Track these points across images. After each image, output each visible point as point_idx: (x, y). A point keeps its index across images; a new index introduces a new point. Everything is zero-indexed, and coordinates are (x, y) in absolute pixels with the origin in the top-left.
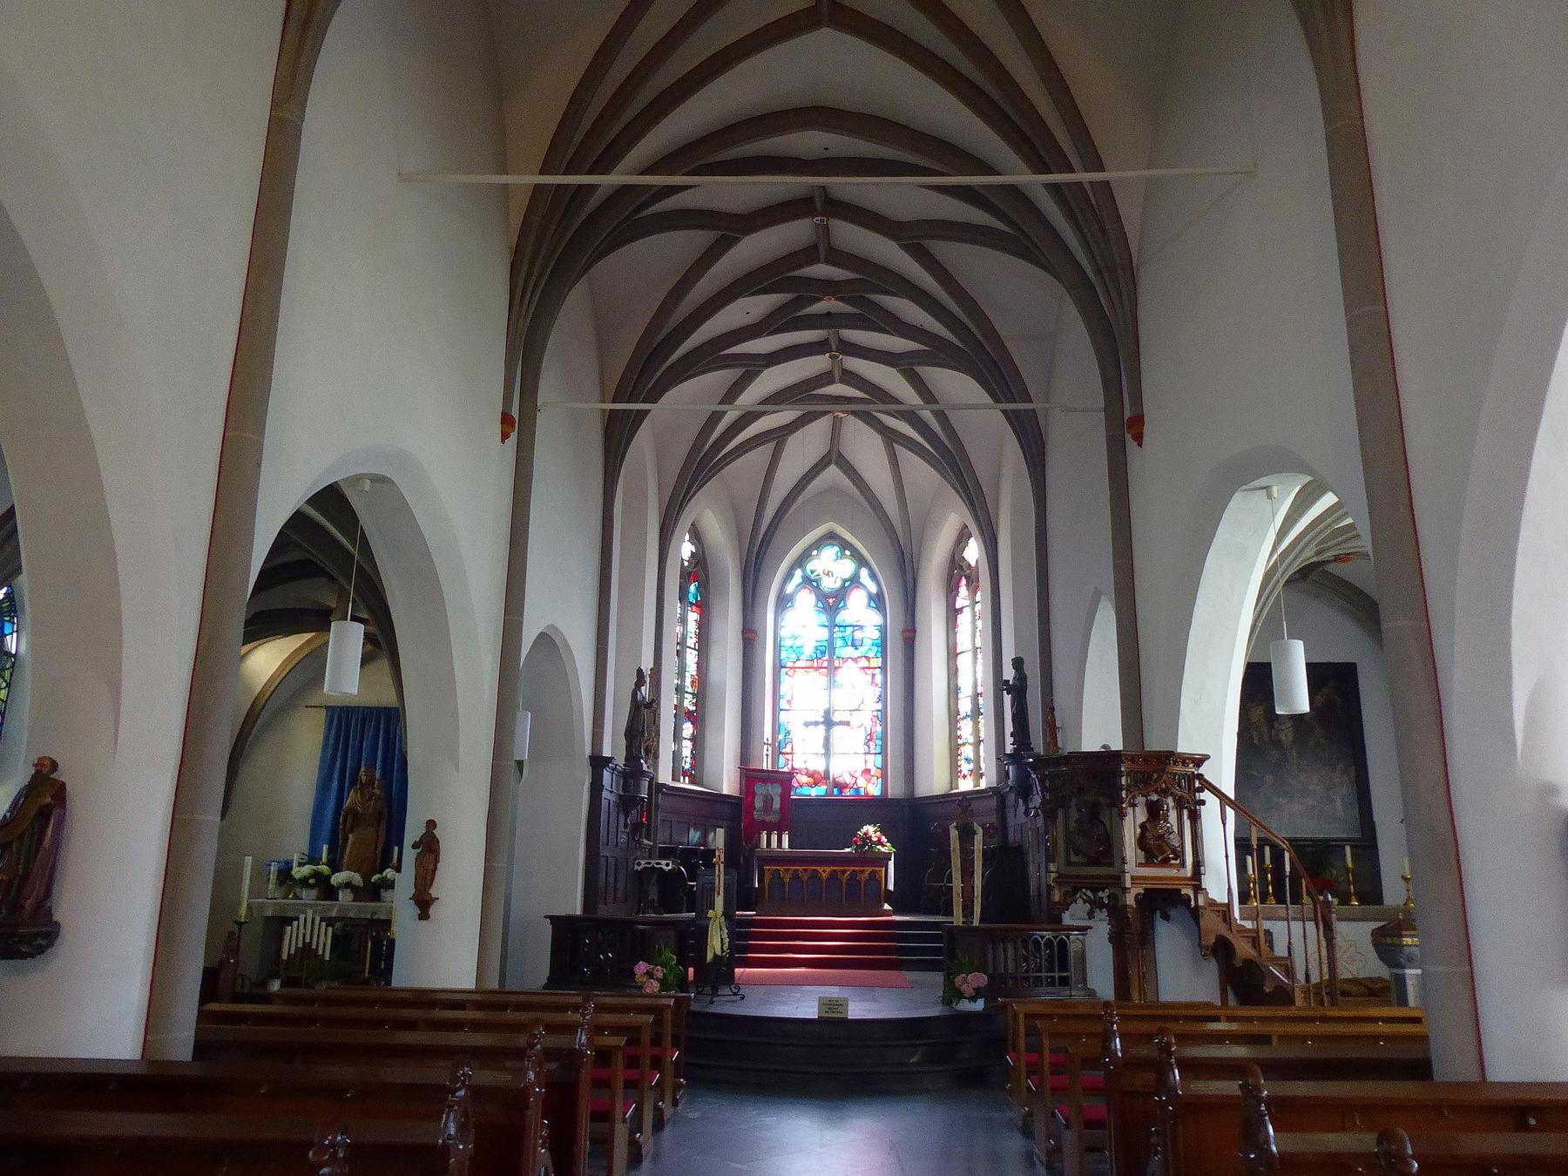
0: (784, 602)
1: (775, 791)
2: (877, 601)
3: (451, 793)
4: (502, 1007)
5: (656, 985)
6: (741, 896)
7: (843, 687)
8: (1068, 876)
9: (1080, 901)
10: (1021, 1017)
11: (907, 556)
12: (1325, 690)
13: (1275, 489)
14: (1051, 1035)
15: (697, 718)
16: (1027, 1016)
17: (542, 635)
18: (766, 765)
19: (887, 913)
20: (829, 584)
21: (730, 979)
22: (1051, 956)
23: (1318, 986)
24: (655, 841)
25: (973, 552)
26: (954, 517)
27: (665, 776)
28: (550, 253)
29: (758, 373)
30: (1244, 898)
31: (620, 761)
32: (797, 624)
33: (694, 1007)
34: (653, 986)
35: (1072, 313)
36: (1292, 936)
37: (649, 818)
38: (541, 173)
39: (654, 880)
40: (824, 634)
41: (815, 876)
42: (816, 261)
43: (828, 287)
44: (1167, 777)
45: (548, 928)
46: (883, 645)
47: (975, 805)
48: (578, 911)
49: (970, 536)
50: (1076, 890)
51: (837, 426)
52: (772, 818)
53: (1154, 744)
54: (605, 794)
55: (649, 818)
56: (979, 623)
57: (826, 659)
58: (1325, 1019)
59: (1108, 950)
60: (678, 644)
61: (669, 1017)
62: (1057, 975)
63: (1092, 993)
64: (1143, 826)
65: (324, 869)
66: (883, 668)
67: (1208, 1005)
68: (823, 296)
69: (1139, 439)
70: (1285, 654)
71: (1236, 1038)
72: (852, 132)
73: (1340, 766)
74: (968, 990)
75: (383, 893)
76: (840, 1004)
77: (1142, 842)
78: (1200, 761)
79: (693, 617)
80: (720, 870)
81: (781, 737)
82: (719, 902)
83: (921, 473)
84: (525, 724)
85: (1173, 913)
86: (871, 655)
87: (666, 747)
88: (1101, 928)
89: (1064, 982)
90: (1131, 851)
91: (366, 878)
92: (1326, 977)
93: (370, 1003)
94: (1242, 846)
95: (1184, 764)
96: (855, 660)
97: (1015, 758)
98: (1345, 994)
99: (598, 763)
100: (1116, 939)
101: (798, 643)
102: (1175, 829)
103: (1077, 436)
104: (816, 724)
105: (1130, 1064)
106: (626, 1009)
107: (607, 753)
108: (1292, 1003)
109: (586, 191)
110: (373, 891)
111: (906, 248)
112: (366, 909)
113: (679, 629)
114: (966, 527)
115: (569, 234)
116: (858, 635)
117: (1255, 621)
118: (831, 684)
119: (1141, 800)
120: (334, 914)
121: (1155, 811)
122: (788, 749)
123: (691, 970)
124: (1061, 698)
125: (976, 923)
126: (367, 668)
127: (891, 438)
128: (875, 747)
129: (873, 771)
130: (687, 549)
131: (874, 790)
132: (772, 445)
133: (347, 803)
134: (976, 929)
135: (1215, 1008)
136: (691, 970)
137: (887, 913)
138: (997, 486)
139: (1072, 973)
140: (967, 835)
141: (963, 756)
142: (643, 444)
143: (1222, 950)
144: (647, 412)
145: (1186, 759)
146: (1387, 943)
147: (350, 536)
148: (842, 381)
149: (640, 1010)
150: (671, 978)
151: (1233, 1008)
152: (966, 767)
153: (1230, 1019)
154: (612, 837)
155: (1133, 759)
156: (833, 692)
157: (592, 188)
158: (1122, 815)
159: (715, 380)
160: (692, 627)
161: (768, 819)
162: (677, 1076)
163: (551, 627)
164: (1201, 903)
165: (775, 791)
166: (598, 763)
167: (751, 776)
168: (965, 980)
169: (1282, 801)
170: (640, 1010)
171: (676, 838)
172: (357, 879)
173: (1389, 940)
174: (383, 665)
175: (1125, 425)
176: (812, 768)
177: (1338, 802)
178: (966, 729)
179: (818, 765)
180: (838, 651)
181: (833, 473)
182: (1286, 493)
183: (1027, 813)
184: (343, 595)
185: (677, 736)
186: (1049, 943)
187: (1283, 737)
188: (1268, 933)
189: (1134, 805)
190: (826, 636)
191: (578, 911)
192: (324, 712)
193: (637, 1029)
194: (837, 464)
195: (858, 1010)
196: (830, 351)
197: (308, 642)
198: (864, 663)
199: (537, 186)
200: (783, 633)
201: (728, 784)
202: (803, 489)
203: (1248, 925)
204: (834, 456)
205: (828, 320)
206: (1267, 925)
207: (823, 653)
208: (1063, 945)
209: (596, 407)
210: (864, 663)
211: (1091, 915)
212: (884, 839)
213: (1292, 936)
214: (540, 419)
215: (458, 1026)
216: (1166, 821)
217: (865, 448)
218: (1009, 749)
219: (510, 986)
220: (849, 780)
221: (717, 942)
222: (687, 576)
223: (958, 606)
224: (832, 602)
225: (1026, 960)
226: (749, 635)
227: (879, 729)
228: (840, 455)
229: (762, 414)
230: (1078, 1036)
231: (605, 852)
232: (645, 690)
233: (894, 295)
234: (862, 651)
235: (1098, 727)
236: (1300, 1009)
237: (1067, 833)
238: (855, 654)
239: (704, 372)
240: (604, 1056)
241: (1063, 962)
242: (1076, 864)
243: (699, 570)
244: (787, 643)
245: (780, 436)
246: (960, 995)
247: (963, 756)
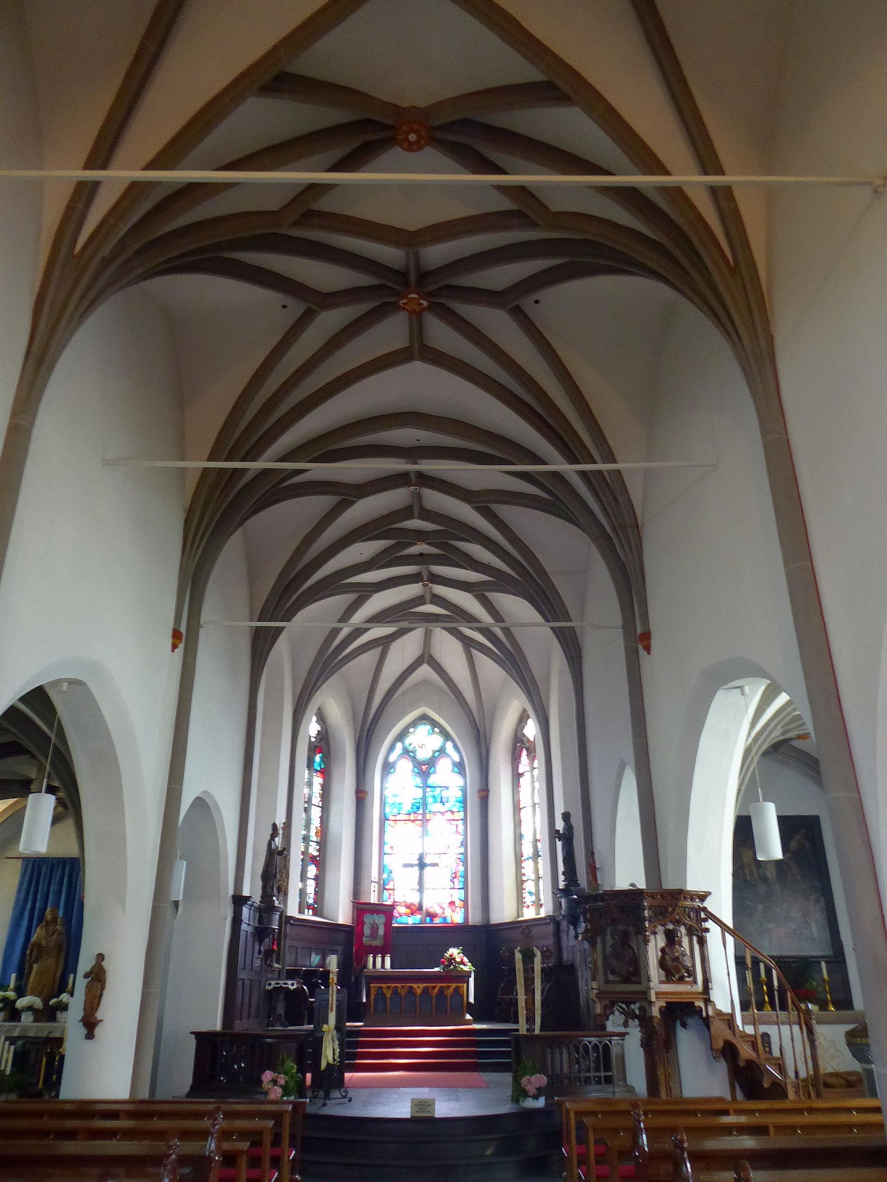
0: (388, 767)
1: (380, 920)
2: (460, 767)
3: (117, 932)
4: (150, 1115)
5: (279, 1090)
6: (352, 1009)
7: (436, 836)
8: (606, 993)
9: (617, 1013)
10: (572, 1115)
11: (481, 733)
12: (798, 837)
13: (746, 688)
14: (595, 1130)
15: (319, 861)
16: (577, 1113)
17: (198, 799)
18: (374, 899)
19: (468, 1023)
20: (423, 755)
21: (340, 1083)
22: (597, 1058)
23: (805, 1080)
24: (283, 966)
25: (531, 730)
26: (515, 703)
27: (292, 910)
28: (214, 514)
29: (369, 597)
30: (745, 1006)
31: (257, 899)
32: (397, 786)
33: (310, 1110)
34: (276, 1093)
35: (596, 555)
36: (785, 1037)
37: (279, 945)
38: (208, 460)
39: (282, 997)
40: (419, 793)
41: (411, 991)
42: (412, 517)
43: (421, 536)
44: (677, 908)
45: (192, 1042)
46: (464, 802)
47: (535, 931)
48: (218, 1027)
49: (529, 717)
50: (613, 1004)
51: (428, 636)
52: (378, 943)
53: (669, 884)
54: (244, 927)
55: (279, 945)
56: (537, 785)
57: (420, 813)
58: (811, 1110)
59: (641, 1052)
60: (306, 803)
61: (287, 1121)
62: (602, 1074)
63: (631, 1090)
64: (663, 950)
65: (11, 994)
66: (465, 820)
67: (721, 1100)
68: (419, 542)
69: (648, 649)
70: (761, 813)
71: (742, 1130)
72: (436, 429)
73: (813, 897)
74: (531, 1090)
75: (59, 1015)
76: (426, 1104)
77: (662, 964)
78: (703, 897)
79: (318, 781)
80: (334, 988)
81: (385, 876)
82: (332, 1017)
83: (490, 670)
84: (181, 870)
85: (690, 1021)
87: (294, 885)
88: (635, 1034)
89: (609, 1080)
90: (654, 971)
91: (46, 1002)
92: (811, 1072)
93: (40, 1115)
94: (740, 962)
95: (692, 899)
96: (443, 814)
97: (566, 892)
98: (827, 1085)
99: (239, 901)
100: (647, 1044)
101: (398, 800)
102: (688, 952)
103: (604, 644)
104: (412, 866)
105: (654, 1157)
106: (250, 1115)
107: (246, 892)
108: (786, 1096)
109: (236, 473)
110: (50, 1013)
111: (476, 509)
112: (44, 1029)
113: (306, 791)
114: (525, 710)
115: (229, 499)
116: (445, 794)
117: (741, 785)
118: (425, 833)
119: (660, 929)
120: (16, 1034)
121: (671, 937)
123: (309, 1076)
124: (599, 845)
125: (537, 1031)
126: (57, 826)
127: (468, 644)
128: (458, 883)
129: (458, 903)
130: (313, 728)
131: (457, 918)
132: (379, 649)
133: (34, 939)
134: (537, 1037)
135: (728, 1103)
136: (309, 1076)
138: (548, 681)
139: (615, 1073)
140: (528, 957)
141: (526, 894)
142: (282, 648)
143: (729, 1052)
144: (281, 629)
145: (692, 896)
146: (858, 1041)
147: (50, 726)
148: (432, 603)
149: (264, 1115)
150: (291, 1084)
151: (741, 1103)
152: (529, 899)
153: (738, 1112)
154: (248, 962)
155: (652, 896)
156: (426, 838)
157: (245, 470)
158: (646, 942)
159: (335, 603)
160: (317, 789)
161: (374, 943)
162: (293, 1173)
163: (205, 792)
164: (710, 1013)
165: (380, 920)
166: (239, 901)
167: (361, 909)
168: (529, 1080)
169: (771, 926)
170: (264, 1115)
171: (301, 961)
172: (37, 1002)
173: (858, 1041)
174: (69, 824)
175: (639, 639)
176: (409, 901)
177: (814, 927)
178: (528, 868)
179: (414, 899)
180: (429, 807)
181: (425, 670)
182: (756, 690)
183: (576, 937)
184: (41, 768)
185: (303, 877)
186: (596, 1047)
187: (768, 874)
188: (766, 1036)
189: (655, 933)
190: (421, 796)
191: (218, 1027)
192: (20, 861)
193: (260, 1133)
194: (429, 664)
195: (446, 1107)
196: (422, 580)
197: (12, 805)
199: (205, 469)
200: (386, 793)
201: (343, 916)
202: (407, 676)
203: (750, 1030)
204: (426, 658)
205: (421, 558)
206: (763, 1029)
207: (418, 808)
208: (606, 1048)
209: (247, 624)
210: (449, 816)
211: (626, 1024)
212: (466, 960)
213: (785, 1037)
214: (203, 633)
215: (110, 1134)
216: (680, 945)
217: (449, 651)
218: (562, 885)
219: (158, 1097)
220: (439, 911)
221: (330, 1052)
222: (314, 749)
223: (520, 771)
224: (425, 769)
225: (578, 1062)
226: (361, 795)
227: (462, 869)
228: (431, 656)
229: (367, 629)
230: (616, 1130)
231: (242, 975)
232: (278, 841)
233: (471, 542)
234: (448, 806)
235: (627, 871)
236: (792, 1102)
237: (605, 957)
238: (443, 809)
239: (328, 596)
240: (230, 1159)
241: (606, 1062)
242: (612, 982)
243: (323, 745)
244: (390, 800)
245: (385, 643)
246: (525, 1094)
247: (526, 894)
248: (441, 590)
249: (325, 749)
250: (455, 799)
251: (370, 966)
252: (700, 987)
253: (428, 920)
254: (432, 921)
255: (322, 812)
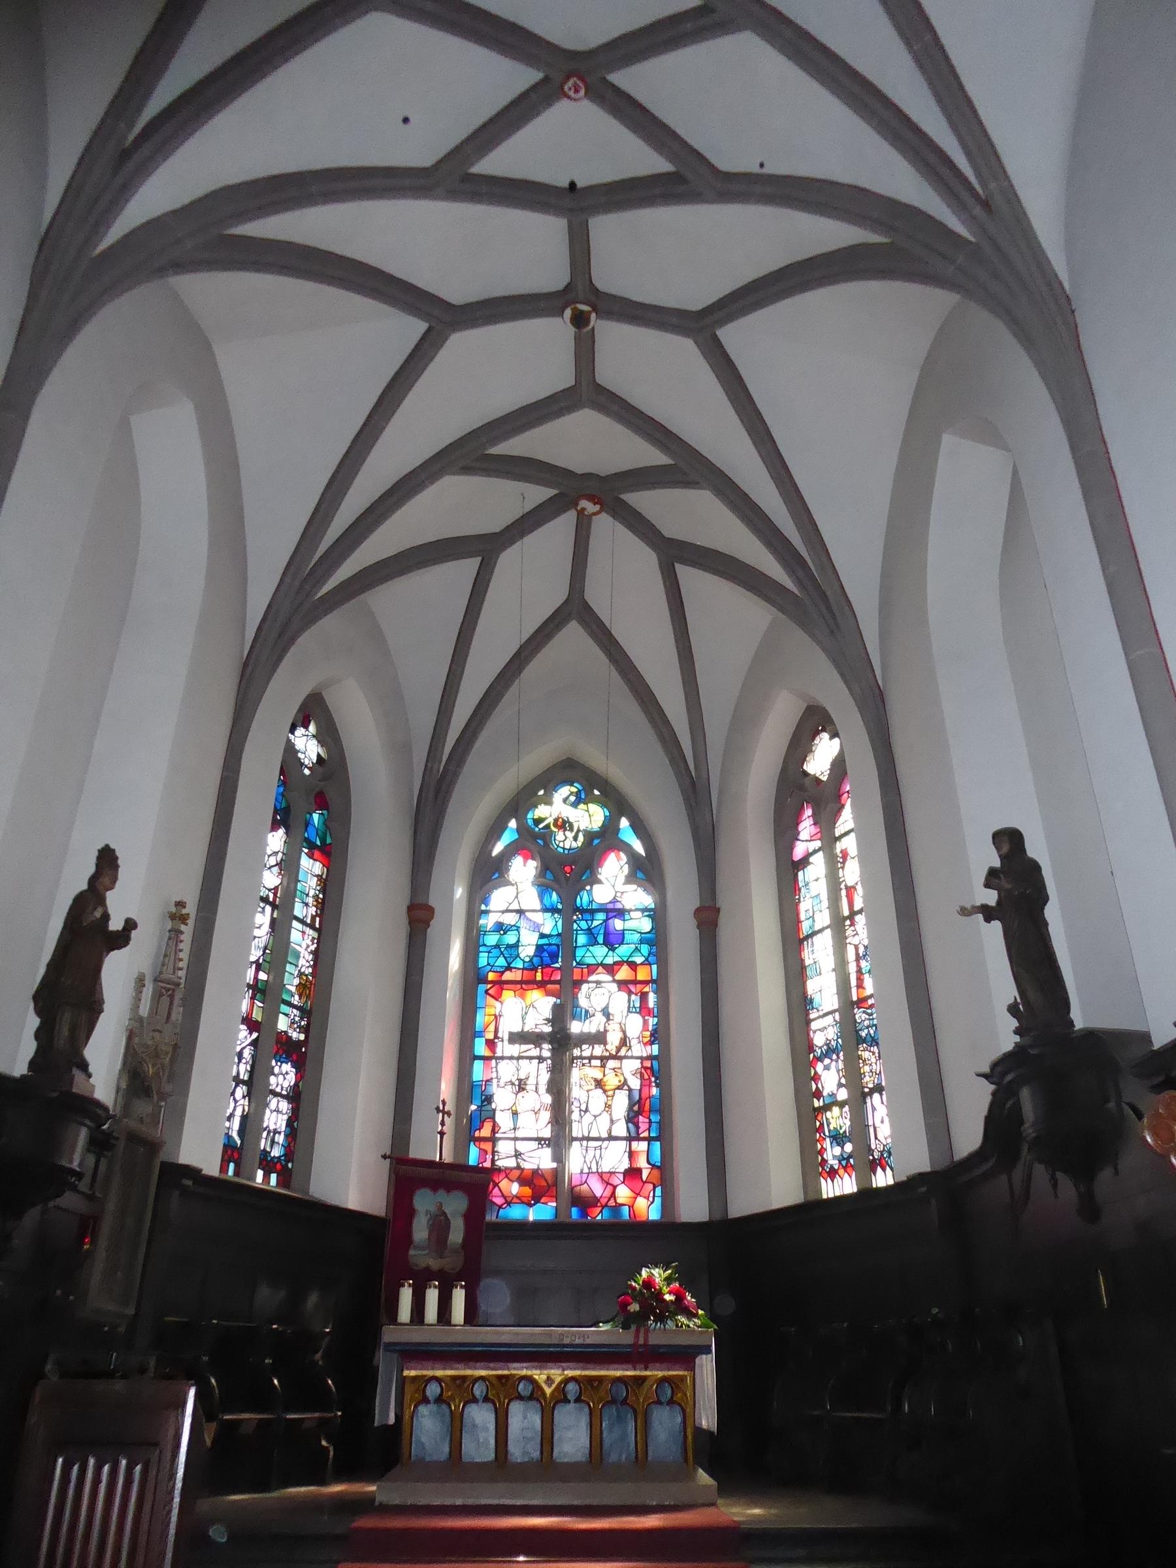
0: (488, 873)
1: (455, 1205)
2: (645, 870)
86: (639, 960)
96: (611, 969)
101: (510, 938)
122: (486, 1132)
165: (455, 1205)
167: (408, 1175)
179: (543, 1160)
180: (579, 953)
181: (573, 633)
198: (624, 973)
201: (350, 1178)
207: (554, 957)
220: (598, 1189)
224: (567, 874)
234: (623, 951)
249: (331, 795)
250: (637, 937)
251: (405, 1312)
253: (575, 1213)
254: (584, 1213)
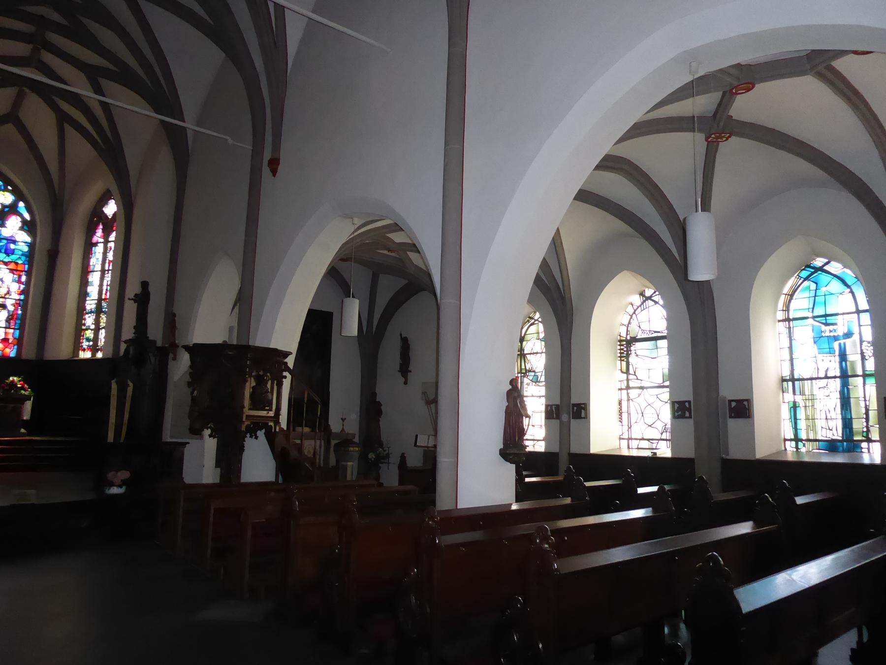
2: (28, 226)
64: (253, 388)
66: (29, 273)
83: (81, 150)
86: (20, 262)
90: (247, 403)
121: (261, 381)
127: (63, 119)
137: (23, 435)
178: (89, 320)
198: (12, 266)
205: (41, 22)
234: (13, 257)
248: (49, 58)
252: (272, 414)
255: (88, 265)
